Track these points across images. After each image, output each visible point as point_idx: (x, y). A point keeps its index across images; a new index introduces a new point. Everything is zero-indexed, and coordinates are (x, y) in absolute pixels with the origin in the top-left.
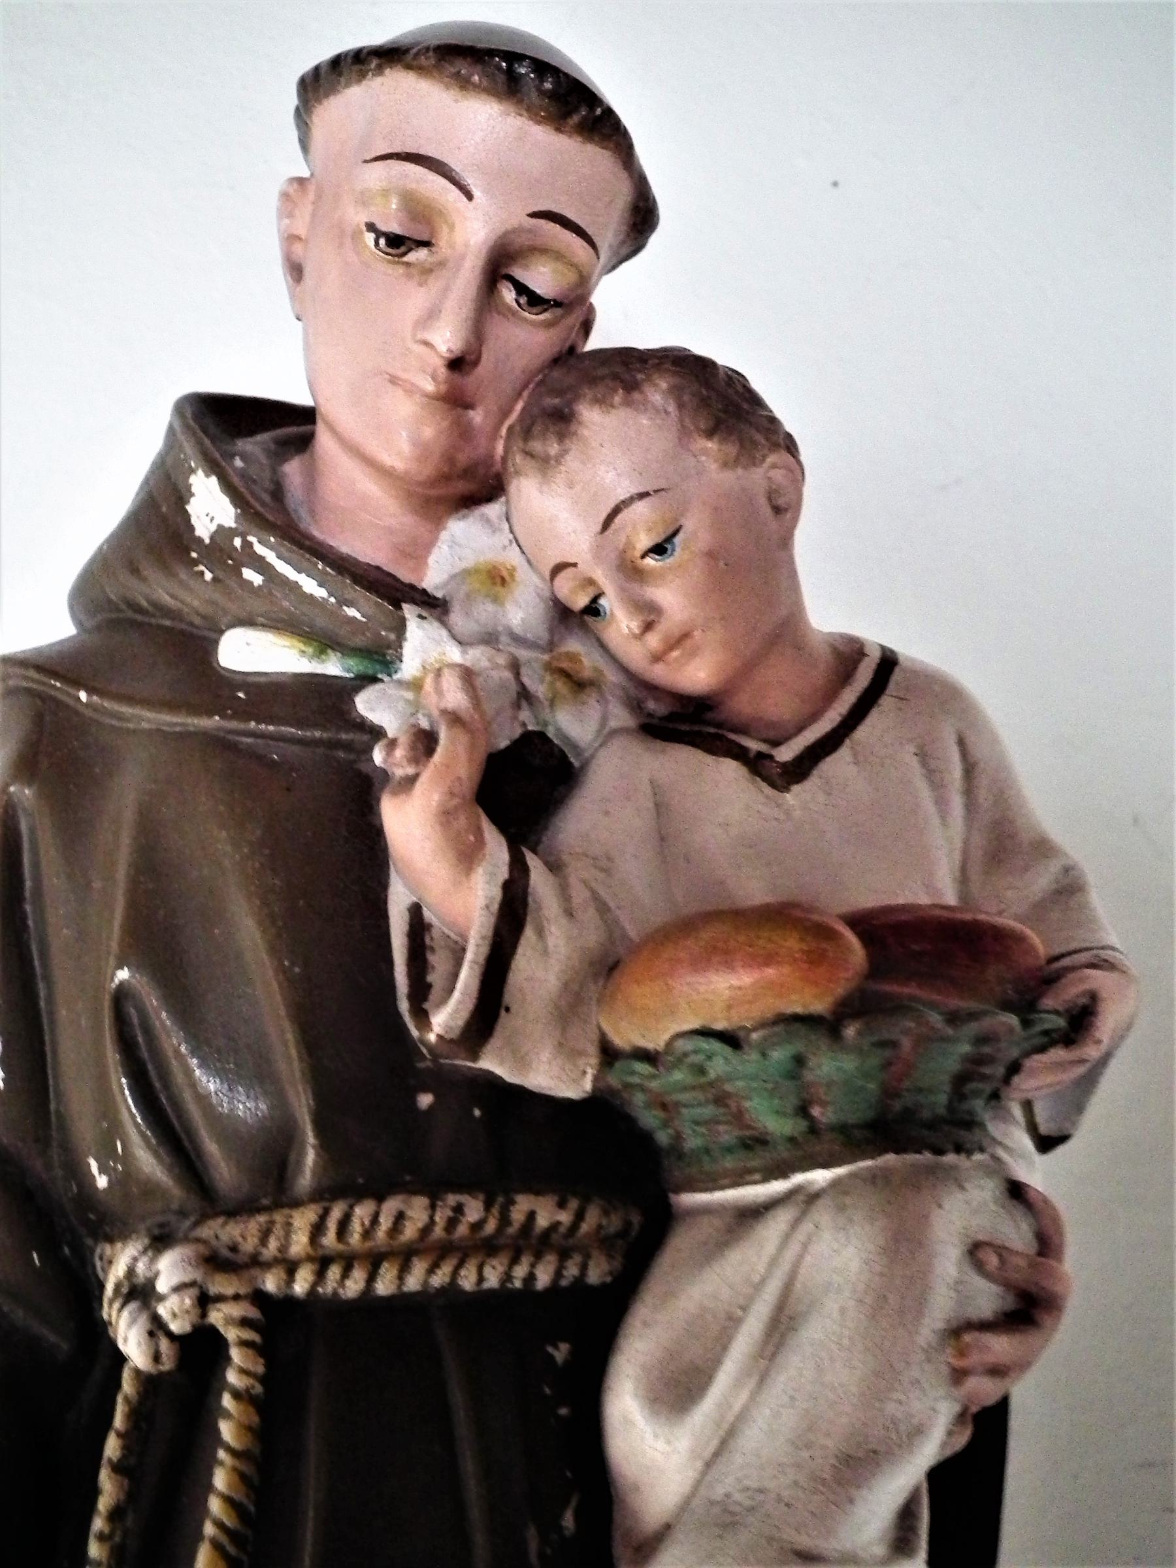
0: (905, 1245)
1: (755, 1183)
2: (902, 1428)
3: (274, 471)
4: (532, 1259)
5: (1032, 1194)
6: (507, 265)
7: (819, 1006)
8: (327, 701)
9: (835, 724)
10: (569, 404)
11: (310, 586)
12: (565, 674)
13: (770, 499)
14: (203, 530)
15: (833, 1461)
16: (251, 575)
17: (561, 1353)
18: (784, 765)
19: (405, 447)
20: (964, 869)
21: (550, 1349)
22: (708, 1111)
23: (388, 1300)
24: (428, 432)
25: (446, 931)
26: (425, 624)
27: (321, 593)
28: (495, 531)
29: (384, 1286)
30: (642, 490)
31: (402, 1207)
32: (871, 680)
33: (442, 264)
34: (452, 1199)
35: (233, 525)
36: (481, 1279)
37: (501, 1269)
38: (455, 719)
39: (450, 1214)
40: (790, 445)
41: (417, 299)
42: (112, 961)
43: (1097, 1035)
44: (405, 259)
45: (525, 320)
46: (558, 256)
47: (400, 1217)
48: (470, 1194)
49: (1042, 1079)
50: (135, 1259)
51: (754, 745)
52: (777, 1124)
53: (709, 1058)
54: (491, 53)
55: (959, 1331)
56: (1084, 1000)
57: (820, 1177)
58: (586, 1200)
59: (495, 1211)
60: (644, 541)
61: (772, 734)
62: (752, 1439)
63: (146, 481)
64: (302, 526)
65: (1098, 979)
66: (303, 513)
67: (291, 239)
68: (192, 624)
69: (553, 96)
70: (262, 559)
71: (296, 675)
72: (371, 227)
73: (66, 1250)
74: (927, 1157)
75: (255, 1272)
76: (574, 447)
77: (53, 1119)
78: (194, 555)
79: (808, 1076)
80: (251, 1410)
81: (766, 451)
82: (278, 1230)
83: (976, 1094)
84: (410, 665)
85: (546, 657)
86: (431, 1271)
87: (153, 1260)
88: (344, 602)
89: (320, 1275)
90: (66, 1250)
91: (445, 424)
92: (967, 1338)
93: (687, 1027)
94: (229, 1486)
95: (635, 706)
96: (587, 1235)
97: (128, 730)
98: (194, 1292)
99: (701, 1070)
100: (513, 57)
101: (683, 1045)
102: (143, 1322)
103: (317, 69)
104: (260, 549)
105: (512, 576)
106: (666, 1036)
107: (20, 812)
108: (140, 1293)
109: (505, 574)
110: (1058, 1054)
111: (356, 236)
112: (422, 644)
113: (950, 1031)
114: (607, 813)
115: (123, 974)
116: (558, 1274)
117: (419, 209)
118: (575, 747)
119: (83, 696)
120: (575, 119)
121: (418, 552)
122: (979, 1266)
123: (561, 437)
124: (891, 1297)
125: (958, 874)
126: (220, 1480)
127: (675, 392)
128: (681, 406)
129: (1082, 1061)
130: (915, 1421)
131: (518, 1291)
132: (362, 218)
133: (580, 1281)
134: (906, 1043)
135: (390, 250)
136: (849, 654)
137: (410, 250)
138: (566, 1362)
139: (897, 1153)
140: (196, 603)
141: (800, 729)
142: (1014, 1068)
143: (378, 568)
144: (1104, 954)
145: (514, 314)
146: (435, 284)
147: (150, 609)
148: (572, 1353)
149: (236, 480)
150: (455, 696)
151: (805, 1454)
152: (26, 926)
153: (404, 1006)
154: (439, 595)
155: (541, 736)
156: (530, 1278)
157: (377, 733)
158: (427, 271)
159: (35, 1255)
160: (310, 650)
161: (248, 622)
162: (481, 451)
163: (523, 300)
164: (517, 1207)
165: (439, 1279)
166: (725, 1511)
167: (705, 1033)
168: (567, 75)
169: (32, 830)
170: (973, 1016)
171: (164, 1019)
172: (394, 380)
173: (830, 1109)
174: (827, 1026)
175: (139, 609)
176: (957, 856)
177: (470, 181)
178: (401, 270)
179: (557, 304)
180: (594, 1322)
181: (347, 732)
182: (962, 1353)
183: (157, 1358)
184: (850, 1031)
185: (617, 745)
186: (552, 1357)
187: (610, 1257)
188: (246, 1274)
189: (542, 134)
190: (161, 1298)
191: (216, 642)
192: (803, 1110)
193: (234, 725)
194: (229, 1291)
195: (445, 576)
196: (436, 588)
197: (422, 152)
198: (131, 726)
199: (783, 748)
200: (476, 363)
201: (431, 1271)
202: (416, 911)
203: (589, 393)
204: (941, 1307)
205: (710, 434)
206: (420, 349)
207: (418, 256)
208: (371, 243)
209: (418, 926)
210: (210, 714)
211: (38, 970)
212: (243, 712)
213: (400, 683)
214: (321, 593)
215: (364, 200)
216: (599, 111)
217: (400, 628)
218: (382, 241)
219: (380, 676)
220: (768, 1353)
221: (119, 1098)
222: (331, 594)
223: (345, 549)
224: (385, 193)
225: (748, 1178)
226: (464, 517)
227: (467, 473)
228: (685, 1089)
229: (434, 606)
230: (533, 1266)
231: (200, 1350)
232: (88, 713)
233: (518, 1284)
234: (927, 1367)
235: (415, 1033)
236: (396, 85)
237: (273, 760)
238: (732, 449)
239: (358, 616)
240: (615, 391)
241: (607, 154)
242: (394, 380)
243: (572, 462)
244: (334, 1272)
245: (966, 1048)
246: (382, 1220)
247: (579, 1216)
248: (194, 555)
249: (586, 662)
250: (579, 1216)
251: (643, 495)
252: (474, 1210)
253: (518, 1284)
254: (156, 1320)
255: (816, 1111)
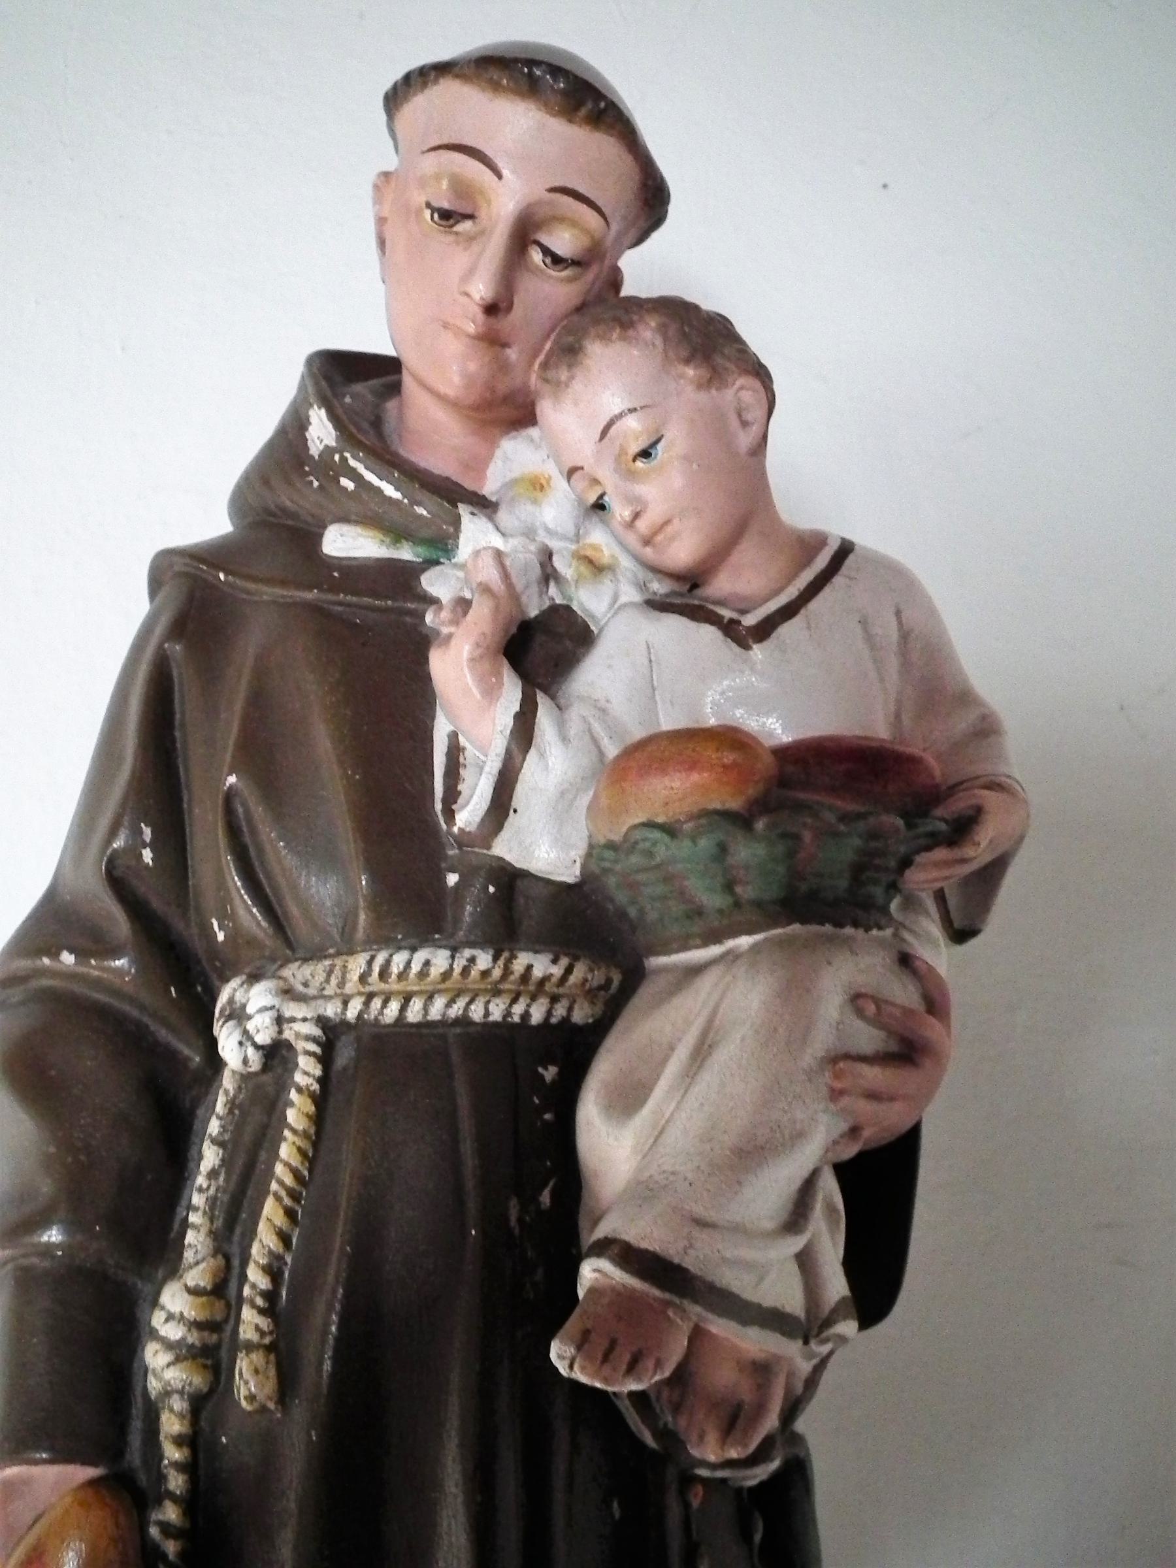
0: (795, 994)
1: (697, 947)
2: (787, 1132)
3: (377, 406)
4: (528, 1001)
5: (918, 963)
6: (535, 232)
7: (735, 804)
8: (400, 581)
9: (793, 597)
10: (579, 341)
11: (389, 490)
12: (590, 561)
13: (740, 416)
14: (315, 449)
15: (728, 1153)
16: (347, 484)
17: (550, 1073)
18: (748, 628)
19: (456, 379)
20: (898, 716)
21: (540, 1070)
22: (660, 889)
23: (418, 1025)
24: (472, 367)
25: (478, 754)
26: (475, 519)
27: (397, 495)
28: (538, 447)
29: (414, 1013)
30: (631, 406)
31: (429, 957)
32: (829, 563)
33: (482, 233)
34: (468, 953)
35: (334, 444)
36: (487, 1013)
37: (503, 1007)
38: (485, 589)
39: (465, 963)
40: (761, 374)
41: (461, 259)
42: (226, 769)
43: (977, 839)
44: (455, 229)
45: (550, 277)
46: (574, 223)
47: (427, 963)
48: (482, 949)
49: (928, 874)
50: (235, 990)
51: (727, 614)
52: (713, 900)
53: (655, 844)
54: (516, 60)
55: (838, 1059)
56: (971, 812)
57: (744, 942)
58: (575, 958)
59: (501, 962)
60: (635, 448)
61: (742, 606)
62: (675, 1137)
63: (283, 418)
64: (393, 448)
65: (990, 799)
66: (395, 437)
67: (381, 221)
68: (306, 522)
69: (565, 93)
70: (354, 470)
71: (378, 560)
72: (428, 205)
73: (199, 989)
74: (828, 928)
75: (320, 1002)
76: (578, 372)
77: (191, 890)
78: (307, 469)
79: (730, 860)
80: (309, 1101)
81: (736, 375)
82: (337, 971)
83: (876, 882)
84: (465, 548)
85: (573, 547)
86: (449, 1005)
87: (247, 991)
88: (415, 502)
89: (367, 1004)
90: (199, 989)
91: (487, 359)
92: (841, 1065)
93: (637, 821)
94: (289, 1156)
95: (642, 587)
96: (575, 985)
97: (256, 602)
98: (273, 1014)
99: (650, 854)
100: (532, 63)
101: (638, 835)
102: (237, 1036)
103: (396, 84)
104: (352, 463)
105: (548, 483)
106: (624, 829)
107: (173, 664)
108: (238, 1014)
109: (544, 482)
110: (940, 854)
111: (419, 213)
112: (475, 534)
113: (842, 828)
114: (610, 666)
115: (232, 779)
116: (549, 1013)
117: (462, 187)
118: (593, 617)
119: (222, 576)
120: (583, 112)
121: (479, 465)
122: (860, 1013)
123: (570, 366)
124: (781, 1030)
125: (892, 719)
126: (285, 1151)
127: (663, 329)
128: (666, 339)
129: (964, 861)
130: (798, 1126)
131: (517, 1024)
132: (422, 199)
133: (566, 1020)
134: (807, 836)
135: (444, 223)
136: (810, 544)
137: (457, 222)
138: (553, 1082)
139: (802, 923)
140: (308, 506)
141: (766, 600)
142: (906, 863)
143: (447, 479)
144: (998, 780)
145: (542, 271)
146: (476, 248)
147: (279, 513)
148: (560, 1074)
149: (339, 411)
150: (489, 573)
151: (708, 1147)
152: (175, 749)
153: (438, 806)
154: (494, 499)
155: (568, 608)
156: (526, 1016)
157: (434, 601)
158: (471, 239)
159: (173, 989)
160: (388, 540)
161: (344, 519)
162: (518, 382)
163: (548, 260)
164: (518, 961)
165: (456, 1010)
166: (647, 1187)
167: (650, 825)
168: (576, 77)
169: (180, 674)
170: (860, 816)
171: (259, 811)
172: (446, 326)
173: (750, 887)
174: (741, 821)
175: (274, 515)
176: (892, 708)
177: (501, 164)
178: (451, 238)
179: (575, 263)
180: (574, 1048)
181: (412, 603)
182: (837, 1076)
183: (245, 1061)
184: (760, 825)
185: (623, 617)
186: (542, 1076)
187: (592, 1003)
188: (313, 1003)
189: (558, 126)
190: (249, 1018)
191: (321, 536)
192: (729, 887)
193: (330, 597)
194: (300, 1016)
195: (499, 484)
196: (492, 494)
197: (464, 143)
198: (256, 598)
199: (749, 616)
200: (510, 308)
201: (449, 1005)
202: (453, 737)
203: (593, 331)
204: (822, 1040)
205: (687, 361)
206: (465, 300)
207: (465, 226)
208: (428, 217)
209: (455, 751)
210: (310, 588)
211: (183, 780)
212: (334, 588)
213: (455, 565)
214: (397, 495)
215: (422, 183)
216: (602, 105)
217: (457, 522)
218: (436, 216)
219: (442, 560)
220: (691, 1074)
221: (226, 871)
222: (404, 497)
223: (423, 464)
224: (438, 177)
225: (691, 942)
226: (515, 438)
227: (507, 399)
228: (638, 871)
229: (485, 505)
230: (528, 1006)
231: (277, 1055)
232: (225, 589)
233: (516, 1019)
234: (808, 1084)
235: (444, 827)
236: (447, 90)
237: (356, 624)
238: (704, 373)
239: (425, 513)
240: (613, 329)
241: (612, 140)
242: (446, 326)
243: (577, 386)
244: (377, 1003)
245: (857, 842)
246: (413, 965)
247: (569, 970)
248: (307, 469)
249: (606, 552)
250: (569, 970)
251: (632, 411)
252: (484, 960)
253: (516, 1019)
254: (245, 1032)
255: (739, 889)
